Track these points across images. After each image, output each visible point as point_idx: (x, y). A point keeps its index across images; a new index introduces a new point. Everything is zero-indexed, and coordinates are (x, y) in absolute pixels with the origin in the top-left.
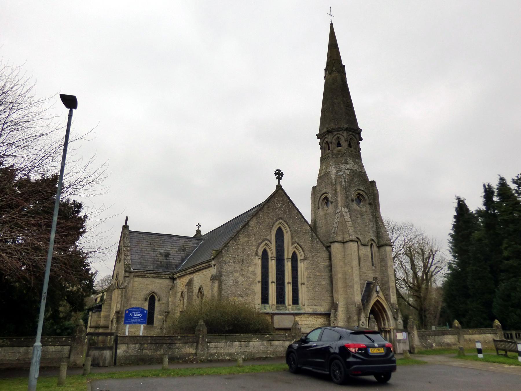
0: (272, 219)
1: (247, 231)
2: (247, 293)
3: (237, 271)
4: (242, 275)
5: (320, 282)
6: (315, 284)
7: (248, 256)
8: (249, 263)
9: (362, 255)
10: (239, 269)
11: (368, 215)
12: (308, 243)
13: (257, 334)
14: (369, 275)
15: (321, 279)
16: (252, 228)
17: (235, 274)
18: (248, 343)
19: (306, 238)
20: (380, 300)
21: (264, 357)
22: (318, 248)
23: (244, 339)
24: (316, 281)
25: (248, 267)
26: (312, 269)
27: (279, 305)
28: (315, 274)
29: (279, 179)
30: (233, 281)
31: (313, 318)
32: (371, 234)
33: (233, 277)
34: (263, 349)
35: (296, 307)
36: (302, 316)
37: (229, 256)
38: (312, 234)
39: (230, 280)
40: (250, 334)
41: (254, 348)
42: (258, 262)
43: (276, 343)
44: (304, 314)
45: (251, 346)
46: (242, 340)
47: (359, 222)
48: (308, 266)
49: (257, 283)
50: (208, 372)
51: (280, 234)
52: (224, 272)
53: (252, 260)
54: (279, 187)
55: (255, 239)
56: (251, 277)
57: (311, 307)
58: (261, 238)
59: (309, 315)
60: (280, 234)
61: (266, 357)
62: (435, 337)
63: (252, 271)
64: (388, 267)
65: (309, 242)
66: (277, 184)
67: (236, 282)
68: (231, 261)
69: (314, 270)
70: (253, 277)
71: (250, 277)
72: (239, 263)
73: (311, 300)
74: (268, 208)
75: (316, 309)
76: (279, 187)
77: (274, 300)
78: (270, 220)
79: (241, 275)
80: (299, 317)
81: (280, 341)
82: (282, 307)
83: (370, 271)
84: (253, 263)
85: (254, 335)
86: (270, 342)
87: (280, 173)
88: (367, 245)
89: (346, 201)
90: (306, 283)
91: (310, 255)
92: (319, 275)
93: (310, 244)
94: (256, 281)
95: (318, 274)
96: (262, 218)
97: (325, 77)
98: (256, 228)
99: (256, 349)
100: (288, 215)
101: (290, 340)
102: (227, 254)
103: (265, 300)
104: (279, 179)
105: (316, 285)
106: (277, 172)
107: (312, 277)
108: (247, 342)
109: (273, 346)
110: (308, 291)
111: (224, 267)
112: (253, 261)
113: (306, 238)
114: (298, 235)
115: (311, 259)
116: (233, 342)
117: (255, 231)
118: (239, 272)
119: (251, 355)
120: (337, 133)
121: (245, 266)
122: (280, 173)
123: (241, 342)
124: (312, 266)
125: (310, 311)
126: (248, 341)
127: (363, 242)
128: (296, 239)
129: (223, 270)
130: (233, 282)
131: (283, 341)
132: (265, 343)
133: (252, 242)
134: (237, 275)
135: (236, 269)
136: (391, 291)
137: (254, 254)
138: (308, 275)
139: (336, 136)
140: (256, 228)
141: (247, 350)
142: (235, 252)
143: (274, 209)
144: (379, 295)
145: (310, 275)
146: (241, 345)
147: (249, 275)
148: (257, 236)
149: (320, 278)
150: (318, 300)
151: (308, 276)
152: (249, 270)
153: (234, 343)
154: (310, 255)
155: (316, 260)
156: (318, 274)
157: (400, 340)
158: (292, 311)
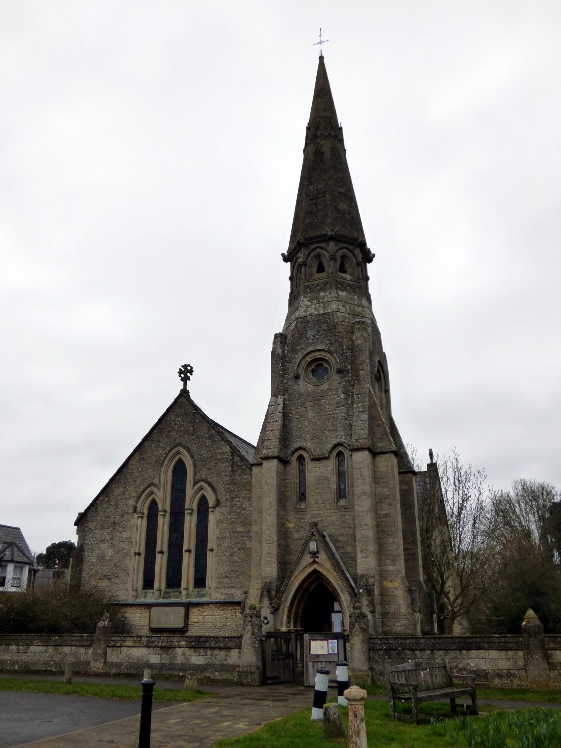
0: (164, 449)
1: (125, 477)
2: (117, 573)
3: (104, 541)
4: (112, 546)
5: (244, 543)
6: (233, 549)
7: (122, 516)
8: (123, 526)
9: (313, 479)
10: (108, 537)
11: (335, 395)
12: (225, 475)
13: (42, 635)
14: (329, 519)
15: (246, 538)
16: (131, 471)
17: (102, 545)
18: (27, 647)
19: (221, 468)
20: (320, 570)
21: (43, 671)
22: (245, 481)
23: (24, 642)
24: (236, 543)
25: (121, 532)
26: (229, 521)
27: (171, 590)
28: (235, 530)
29: (185, 379)
30: (99, 556)
31: (226, 610)
32: (339, 433)
33: (98, 550)
34: (46, 657)
35: (198, 592)
36: (206, 607)
37: (97, 520)
38: (233, 459)
39: (94, 555)
40: (33, 635)
41: (34, 656)
42: (143, 524)
43: (66, 650)
44: (208, 604)
45: (31, 652)
46: (20, 642)
47: (310, 414)
48: (221, 518)
49: (133, 556)
50: (482, 714)
51: (180, 469)
52: (87, 544)
53: (128, 520)
54: (184, 393)
55: (135, 487)
56: (125, 547)
57: (223, 590)
58: (144, 484)
59: (218, 605)
60: (180, 469)
61: (46, 671)
62: (432, 653)
63: (126, 539)
64: (356, 497)
65: (228, 473)
66: (182, 387)
67: (101, 558)
68: (98, 527)
69: (232, 522)
70: (127, 547)
71: (123, 548)
72: (109, 527)
73: (224, 578)
74: (160, 432)
75: (232, 594)
76: (184, 393)
77: (209, 578)
78: (161, 451)
79: (111, 546)
80: (199, 609)
81: (72, 646)
82: (174, 592)
83: (330, 511)
84: (130, 525)
85: (38, 636)
86: (57, 647)
87: (183, 369)
88: (327, 458)
89: (282, 383)
90: (215, 549)
91: (227, 497)
92: (242, 532)
93: (227, 478)
94: (132, 553)
95: (240, 529)
96: (149, 451)
97: (304, 150)
98: (138, 469)
99: (36, 657)
100: (193, 435)
101: (88, 646)
102: (94, 517)
103: (148, 583)
104: (185, 379)
105: (236, 550)
106: (189, 368)
107: (227, 536)
108: (26, 646)
109: (60, 654)
110: (219, 563)
111: (88, 536)
112: (129, 523)
113: (221, 468)
114: (207, 466)
115: (228, 504)
116: (9, 645)
117: (136, 475)
118: (108, 542)
119: (26, 666)
120: (315, 245)
121: (117, 532)
122: (183, 369)
123: (19, 645)
124: (229, 517)
125: (221, 598)
126: (27, 645)
127: (317, 454)
128: (203, 474)
129: (86, 542)
130: (98, 557)
131: (76, 647)
132: (51, 649)
133: (130, 492)
134: (104, 546)
135: (103, 537)
136: (358, 549)
137: (131, 511)
138: (220, 533)
139: (313, 254)
140: (138, 469)
141: (25, 658)
142: (105, 512)
143: (169, 431)
144: (316, 560)
145: (226, 533)
146: (18, 649)
147: (121, 545)
148: (138, 482)
149: (244, 536)
150: (237, 577)
151: (221, 536)
152: (121, 537)
153: (10, 647)
154: (227, 497)
155: (239, 504)
156: (240, 529)
157: (318, 656)
158: (187, 599)
